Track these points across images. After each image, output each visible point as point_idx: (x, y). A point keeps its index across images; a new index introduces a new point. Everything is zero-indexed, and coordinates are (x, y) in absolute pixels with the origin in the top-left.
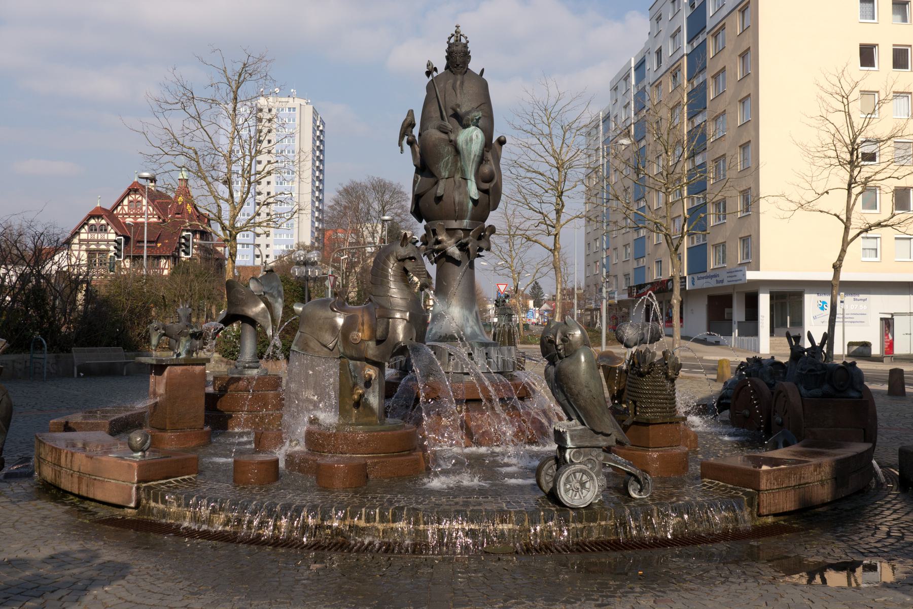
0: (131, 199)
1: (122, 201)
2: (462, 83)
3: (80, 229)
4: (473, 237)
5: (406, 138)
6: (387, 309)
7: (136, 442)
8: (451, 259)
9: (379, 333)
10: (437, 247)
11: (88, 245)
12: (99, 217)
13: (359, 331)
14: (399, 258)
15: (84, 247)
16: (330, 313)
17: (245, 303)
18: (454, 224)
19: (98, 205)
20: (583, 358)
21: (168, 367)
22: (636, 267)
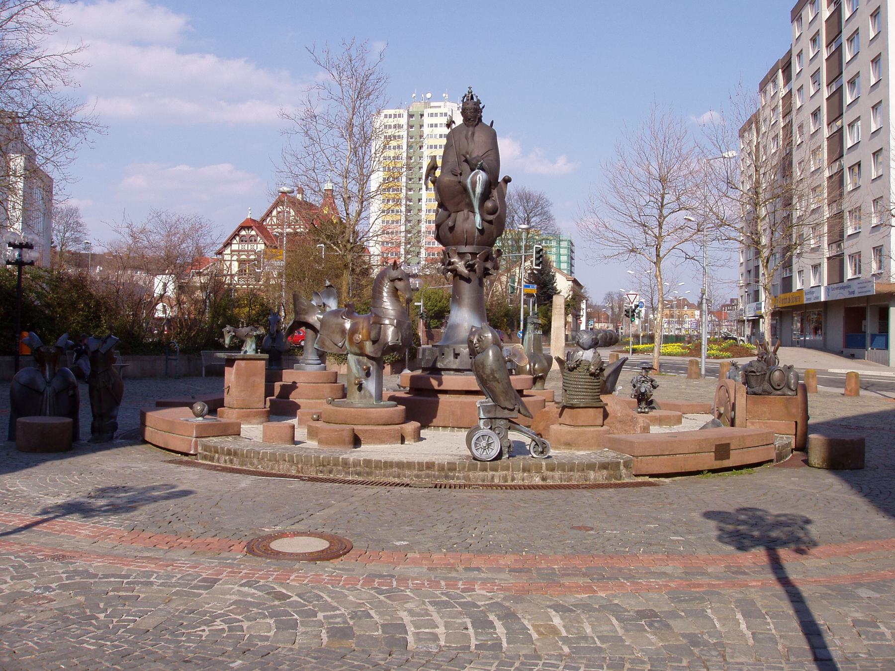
0: (279, 210)
1: (271, 212)
2: (473, 134)
3: (231, 240)
4: (480, 259)
5: (430, 178)
6: (380, 317)
7: (197, 410)
8: (462, 277)
9: (373, 335)
10: (450, 267)
11: (239, 256)
12: (249, 228)
13: (360, 334)
14: (391, 279)
15: (235, 258)
16: (340, 320)
17: (306, 312)
18: (464, 249)
19: (249, 217)
20: (491, 353)
21: (236, 362)
22: (785, 276)
